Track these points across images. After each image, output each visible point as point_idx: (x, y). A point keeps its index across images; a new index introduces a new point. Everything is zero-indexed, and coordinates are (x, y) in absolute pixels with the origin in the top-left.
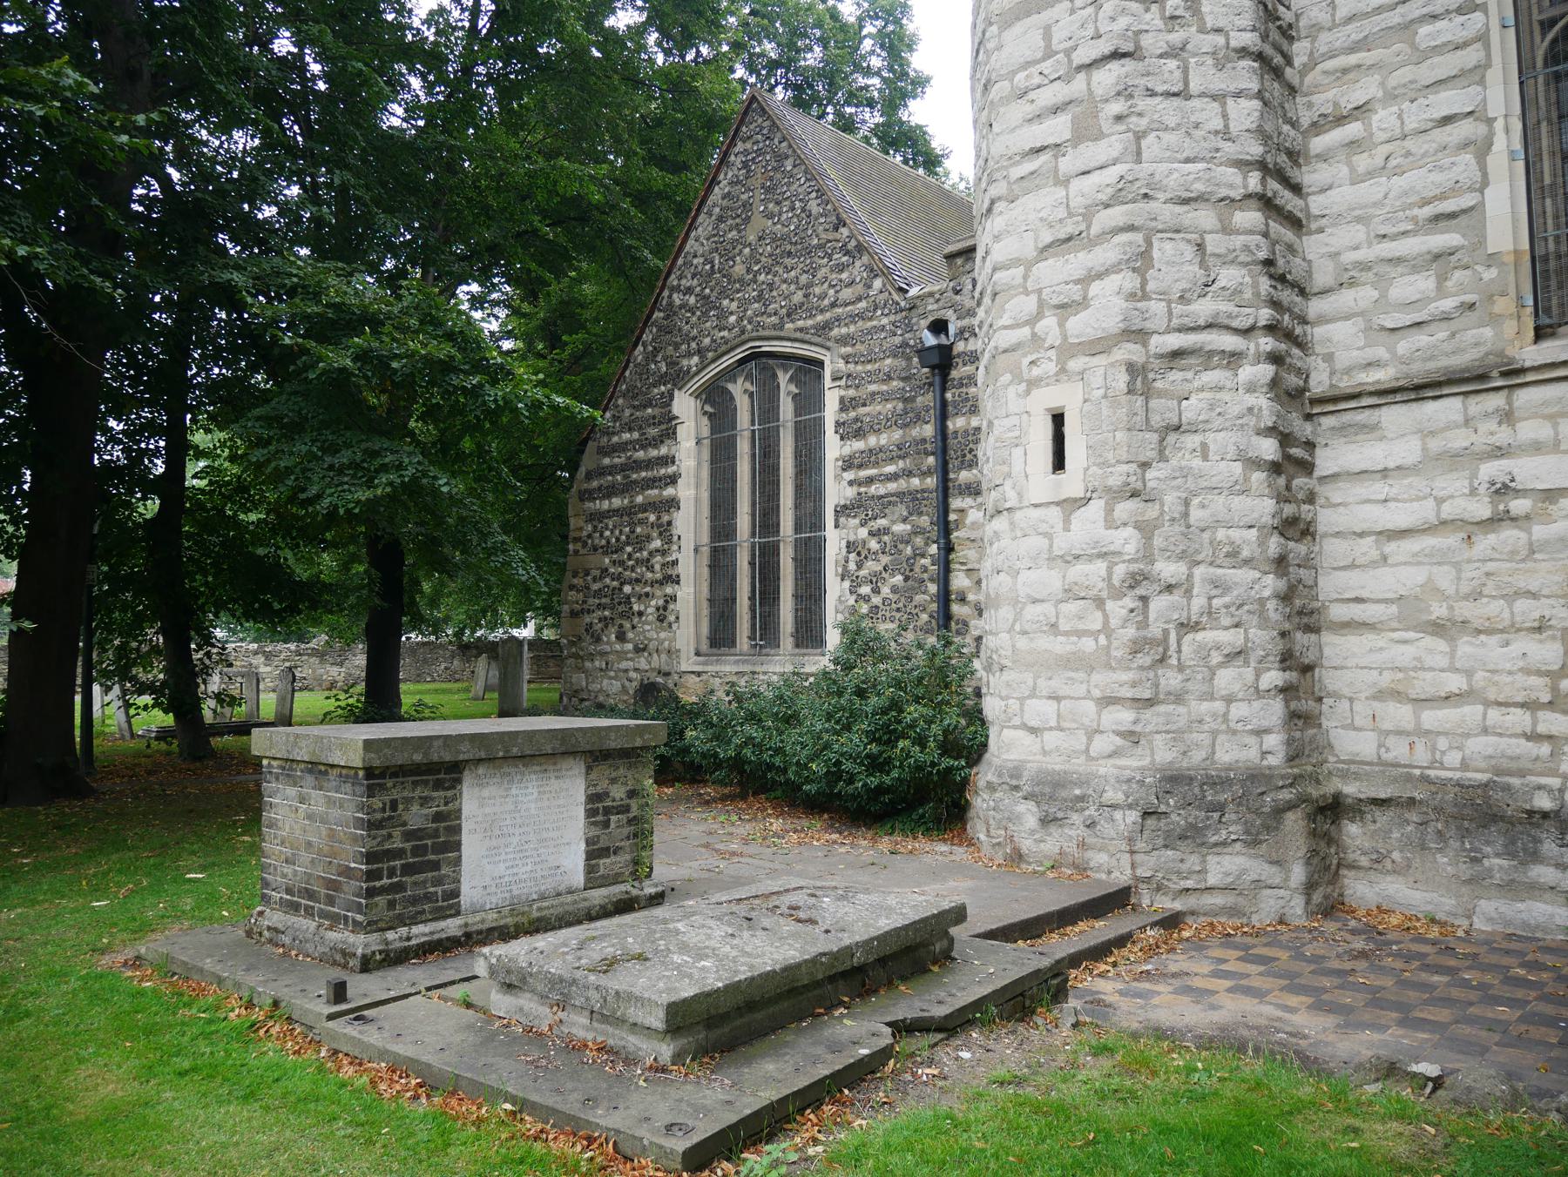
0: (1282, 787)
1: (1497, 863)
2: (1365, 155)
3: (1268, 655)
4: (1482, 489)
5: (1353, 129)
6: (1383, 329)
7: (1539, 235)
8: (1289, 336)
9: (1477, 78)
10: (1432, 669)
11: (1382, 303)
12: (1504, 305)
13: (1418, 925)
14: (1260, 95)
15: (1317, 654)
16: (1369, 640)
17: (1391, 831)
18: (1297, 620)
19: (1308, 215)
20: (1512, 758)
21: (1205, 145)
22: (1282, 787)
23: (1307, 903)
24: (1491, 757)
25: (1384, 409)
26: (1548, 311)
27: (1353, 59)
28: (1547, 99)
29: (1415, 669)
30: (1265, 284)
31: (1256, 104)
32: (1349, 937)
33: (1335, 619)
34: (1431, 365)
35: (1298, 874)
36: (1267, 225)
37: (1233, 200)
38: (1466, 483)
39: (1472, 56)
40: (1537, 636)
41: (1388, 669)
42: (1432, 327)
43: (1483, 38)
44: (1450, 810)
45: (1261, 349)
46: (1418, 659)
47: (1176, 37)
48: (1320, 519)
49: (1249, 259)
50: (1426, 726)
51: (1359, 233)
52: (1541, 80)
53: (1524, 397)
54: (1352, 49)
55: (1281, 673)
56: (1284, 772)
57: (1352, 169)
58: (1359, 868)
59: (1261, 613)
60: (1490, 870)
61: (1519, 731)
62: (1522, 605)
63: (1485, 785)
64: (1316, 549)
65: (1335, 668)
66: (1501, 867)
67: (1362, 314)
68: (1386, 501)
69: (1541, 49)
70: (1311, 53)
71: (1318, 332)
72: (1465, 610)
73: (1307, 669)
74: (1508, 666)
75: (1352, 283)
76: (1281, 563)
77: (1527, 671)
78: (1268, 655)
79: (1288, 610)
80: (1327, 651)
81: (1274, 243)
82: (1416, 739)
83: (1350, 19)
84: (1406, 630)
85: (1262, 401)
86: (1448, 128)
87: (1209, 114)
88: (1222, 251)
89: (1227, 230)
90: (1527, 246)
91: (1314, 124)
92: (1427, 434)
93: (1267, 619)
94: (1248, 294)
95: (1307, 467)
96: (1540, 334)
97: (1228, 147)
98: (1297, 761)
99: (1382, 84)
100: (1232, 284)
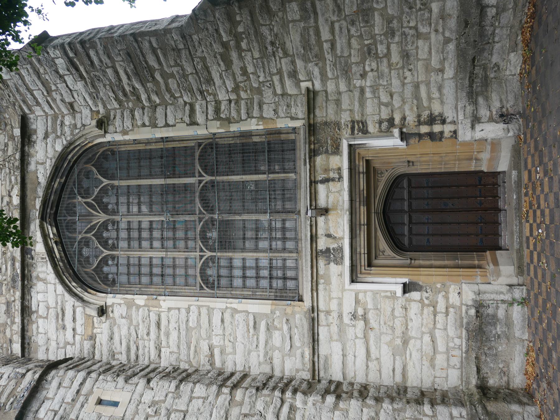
0: (476, 410)
1: (499, 329)
2: (227, 349)
3: (417, 410)
4: (353, 323)
5: (217, 352)
6: (290, 350)
7: (268, 297)
8: (287, 385)
9: (212, 310)
10: (422, 346)
11: (281, 349)
12: (289, 310)
13: (530, 360)
14: (195, 383)
15: (416, 389)
16: (410, 368)
17: (491, 367)
18: (402, 396)
19: (243, 371)
20: (456, 321)
21: (207, 407)
22: (476, 410)
23: (529, 405)
24: (456, 328)
25: (320, 353)
26: (294, 297)
27: (192, 348)
28: (225, 291)
29: (422, 352)
30: (265, 392)
31: (198, 385)
32: (541, 389)
33: (401, 380)
34: (306, 335)
35: (515, 407)
36: (243, 388)
37: (231, 400)
38: (350, 328)
39: (204, 311)
40: (409, 310)
41: (422, 362)
42: (293, 333)
43: (199, 307)
44: (479, 344)
45: (290, 397)
46: (418, 350)
47: (163, 412)
48: (360, 382)
49: (255, 397)
50: (445, 350)
51: (254, 354)
52: (218, 292)
53: (322, 306)
54: (189, 348)
55: (425, 405)
56: (469, 409)
57: (231, 354)
58: (508, 381)
59: (399, 410)
60: (502, 332)
61: (445, 318)
62: (397, 313)
63: (467, 331)
64: (372, 384)
65: (422, 382)
66: (501, 328)
67: (283, 357)
68: (355, 356)
69: (208, 290)
70: (186, 362)
71: (287, 373)
72: (398, 332)
73: (423, 394)
74: (420, 320)
75: (271, 359)
76: (378, 400)
77: (422, 314)
78: (417, 410)
79: (397, 399)
80: (415, 385)
81: (250, 386)
82: (450, 354)
83: (179, 347)
84: (406, 354)
85: (311, 399)
86: (225, 321)
87: (197, 404)
88: (249, 407)
89: (241, 404)
90: (271, 301)
91: (211, 365)
92: (331, 339)
93: (402, 408)
94: (268, 399)
95: (339, 384)
96: (301, 300)
97: (210, 399)
98: (463, 402)
99: (204, 340)
100: (263, 405)
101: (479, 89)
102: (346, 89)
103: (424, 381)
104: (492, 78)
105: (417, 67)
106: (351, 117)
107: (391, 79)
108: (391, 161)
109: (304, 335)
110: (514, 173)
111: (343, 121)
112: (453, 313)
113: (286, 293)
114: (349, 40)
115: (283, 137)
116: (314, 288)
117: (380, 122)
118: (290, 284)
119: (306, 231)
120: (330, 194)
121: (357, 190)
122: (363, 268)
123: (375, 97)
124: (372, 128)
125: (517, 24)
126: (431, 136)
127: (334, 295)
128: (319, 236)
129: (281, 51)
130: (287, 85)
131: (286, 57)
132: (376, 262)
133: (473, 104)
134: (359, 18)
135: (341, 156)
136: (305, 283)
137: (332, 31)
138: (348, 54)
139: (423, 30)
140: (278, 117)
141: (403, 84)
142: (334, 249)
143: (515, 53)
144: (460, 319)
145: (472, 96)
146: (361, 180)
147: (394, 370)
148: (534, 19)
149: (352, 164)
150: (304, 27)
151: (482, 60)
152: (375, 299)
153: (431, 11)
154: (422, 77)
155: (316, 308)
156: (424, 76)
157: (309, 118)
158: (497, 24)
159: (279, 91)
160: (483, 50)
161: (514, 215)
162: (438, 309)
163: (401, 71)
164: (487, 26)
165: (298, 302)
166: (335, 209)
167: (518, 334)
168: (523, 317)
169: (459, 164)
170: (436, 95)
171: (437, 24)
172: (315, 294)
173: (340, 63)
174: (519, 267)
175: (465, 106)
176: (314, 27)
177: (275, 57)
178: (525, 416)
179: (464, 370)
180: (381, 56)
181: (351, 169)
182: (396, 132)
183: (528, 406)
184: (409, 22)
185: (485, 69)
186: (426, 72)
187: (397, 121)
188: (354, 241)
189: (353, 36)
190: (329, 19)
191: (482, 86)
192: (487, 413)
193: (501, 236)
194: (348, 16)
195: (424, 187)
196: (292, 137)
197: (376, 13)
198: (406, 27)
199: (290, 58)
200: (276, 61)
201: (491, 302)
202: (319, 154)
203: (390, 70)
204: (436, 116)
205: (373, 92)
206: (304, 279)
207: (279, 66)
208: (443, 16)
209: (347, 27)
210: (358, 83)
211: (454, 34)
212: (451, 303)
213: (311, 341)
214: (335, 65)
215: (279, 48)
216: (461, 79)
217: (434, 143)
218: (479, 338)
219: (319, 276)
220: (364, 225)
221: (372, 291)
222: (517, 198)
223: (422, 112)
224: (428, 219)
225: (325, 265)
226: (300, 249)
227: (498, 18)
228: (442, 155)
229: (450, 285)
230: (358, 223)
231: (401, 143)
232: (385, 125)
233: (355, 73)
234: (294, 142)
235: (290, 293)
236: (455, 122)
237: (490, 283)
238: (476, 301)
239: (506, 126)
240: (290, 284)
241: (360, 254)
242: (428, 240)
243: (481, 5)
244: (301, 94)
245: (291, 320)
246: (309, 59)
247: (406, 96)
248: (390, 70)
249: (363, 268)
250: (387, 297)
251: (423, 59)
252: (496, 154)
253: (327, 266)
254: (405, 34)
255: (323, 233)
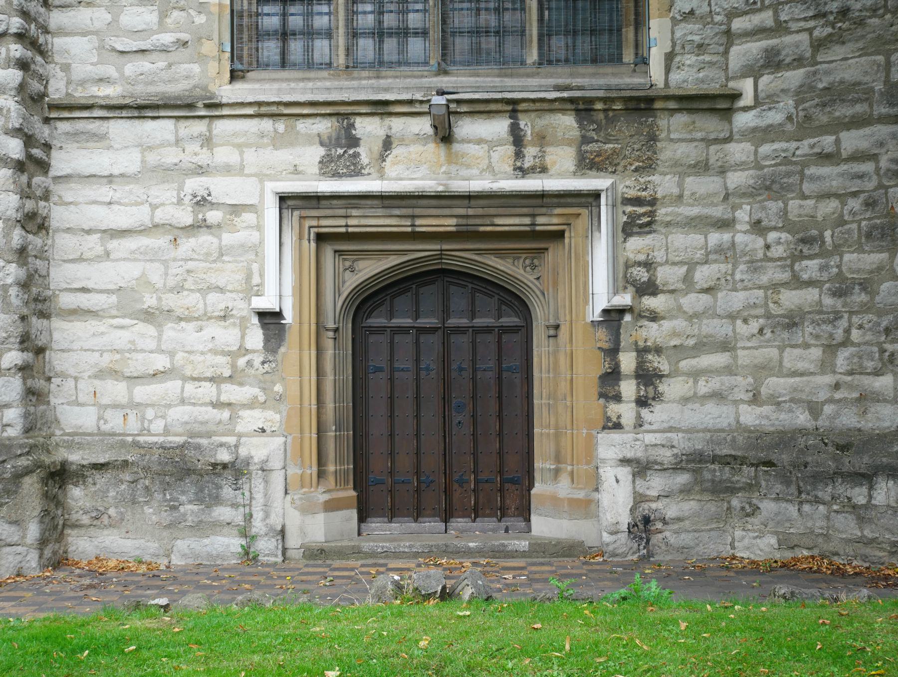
0: (20, 455)
1: (189, 509)
3: (9, 337)
4: (187, 200)
6: (114, 50)
8: (34, 45)
10: (143, 351)
11: (113, 25)
12: (209, 48)
15: (48, 338)
17: (108, 490)
20: (202, 423)
22: (20, 455)
23: (40, 557)
24: (187, 423)
25: (112, 122)
26: (240, 58)
29: (130, 351)
33: (63, 307)
34: (152, 89)
35: (33, 531)
38: (175, 193)
40: (222, 323)
41: (108, 351)
42: (154, 56)
44: (155, 468)
46: (132, 342)
48: (53, 214)
50: (137, 399)
53: (221, 126)
55: (20, 353)
56: (21, 442)
60: (185, 515)
61: (208, 400)
62: (212, 297)
63: (182, 446)
64: (50, 242)
65: (63, 351)
67: (96, 33)
68: (110, 203)
71: (58, 43)
72: (171, 301)
73: (40, 351)
74: (201, 348)
76: (22, 253)
77: (214, 351)
78: (9, 337)
80: (56, 336)
82: (129, 411)
84: (124, 317)
93: (9, 304)
95: (43, 166)
96: (234, 76)
101: (707, 476)
102: (731, 186)
103: (65, 355)
104: (729, 502)
105: (767, 347)
106: (664, 197)
107: (745, 289)
108: (560, 288)
109: (152, 83)
110: (523, 545)
111: (655, 178)
112: (218, 417)
113: (250, 41)
114: (837, 196)
115: (629, 33)
116: (264, 110)
117: (648, 265)
118: (270, 49)
119: (401, 90)
120: (486, 147)
121: (492, 211)
122: (314, 223)
123: (708, 254)
124: (636, 246)
125: (831, 547)
126: (612, 376)
127: (250, 156)
128: (388, 121)
129: (825, 34)
130: (749, 45)
131: (812, 46)
132: (328, 251)
133: (676, 464)
134: (878, 217)
135: (574, 173)
136: (276, 86)
137: (858, 157)
138: (807, 193)
139: (842, 359)
140: (675, 22)
141: (732, 317)
142: (356, 155)
143: (776, 546)
144: (208, 432)
145: (693, 461)
146: (517, 221)
147: (84, 290)
148: (832, 574)
149: (555, 200)
150: (872, 90)
151: (767, 481)
152: (244, 248)
153: (877, 373)
154: (744, 357)
155: (217, 113)
156: (747, 361)
157: (667, 98)
158: (835, 507)
159: (738, 24)
160: (787, 483)
161: (434, 543)
162: (226, 387)
163: (760, 311)
164: (834, 487)
165: (228, 68)
166: (452, 159)
167: (182, 545)
168: (218, 556)
169: (548, 435)
170: (703, 387)
171: (851, 387)
172: (250, 111)
173: (788, 174)
174: (322, 551)
175: (673, 447)
176: (871, 115)
177: (814, 17)
178: (19, 549)
179: (97, 438)
180: (797, 267)
181: (541, 198)
182: (625, 299)
183: (37, 556)
184: (861, 327)
185: (750, 487)
186: (756, 366)
187: (650, 302)
188: (375, 202)
189: (844, 204)
190: (883, 151)
191: (713, 481)
192: (18, 476)
193: (390, 522)
194: (886, 193)
195: (499, 361)
196: (628, 56)
197: (884, 256)
198: (850, 321)
199: (808, 55)
200: (805, 19)
201: (247, 494)
202: (580, 122)
203: (765, 288)
204: (656, 388)
205: (719, 250)
206: (284, 85)
207: (794, 26)
208: (865, 399)
209: (863, 192)
210: (743, 215)
211: (827, 424)
212: (241, 413)
213: (139, 101)
214: (786, 161)
215: (833, 28)
216: (734, 440)
217: (597, 381)
218: (169, 468)
219: (293, 120)
220: (413, 225)
221: (262, 242)
222: (470, 548)
223: (668, 358)
224: (427, 369)
225: (319, 135)
226: (356, 74)
227: (846, 509)
228: (569, 399)
229: (280, 412)
230: (417, 211)
231: (598, 310)
232: (642, 275)
233: (764, 208)
234: (616, 59)
235: (250, 49)
236: (641, 426)
237: (286, 493)
238: (248, 464)
239: (625, 527)
240: (270, 49)
241: (346, 217)
242: (379, 370)
243: (875, 474)
244: (728, 79)
245: (185, 53)
246: (803, 101)
247: (705, 321)
248: (765, 288)
249: (314, 223)
250: (249, 277)
251: (781, 357)
252: (566, 509)
253: (317, 139)
254: (836, 319)
255: (393, 131)
